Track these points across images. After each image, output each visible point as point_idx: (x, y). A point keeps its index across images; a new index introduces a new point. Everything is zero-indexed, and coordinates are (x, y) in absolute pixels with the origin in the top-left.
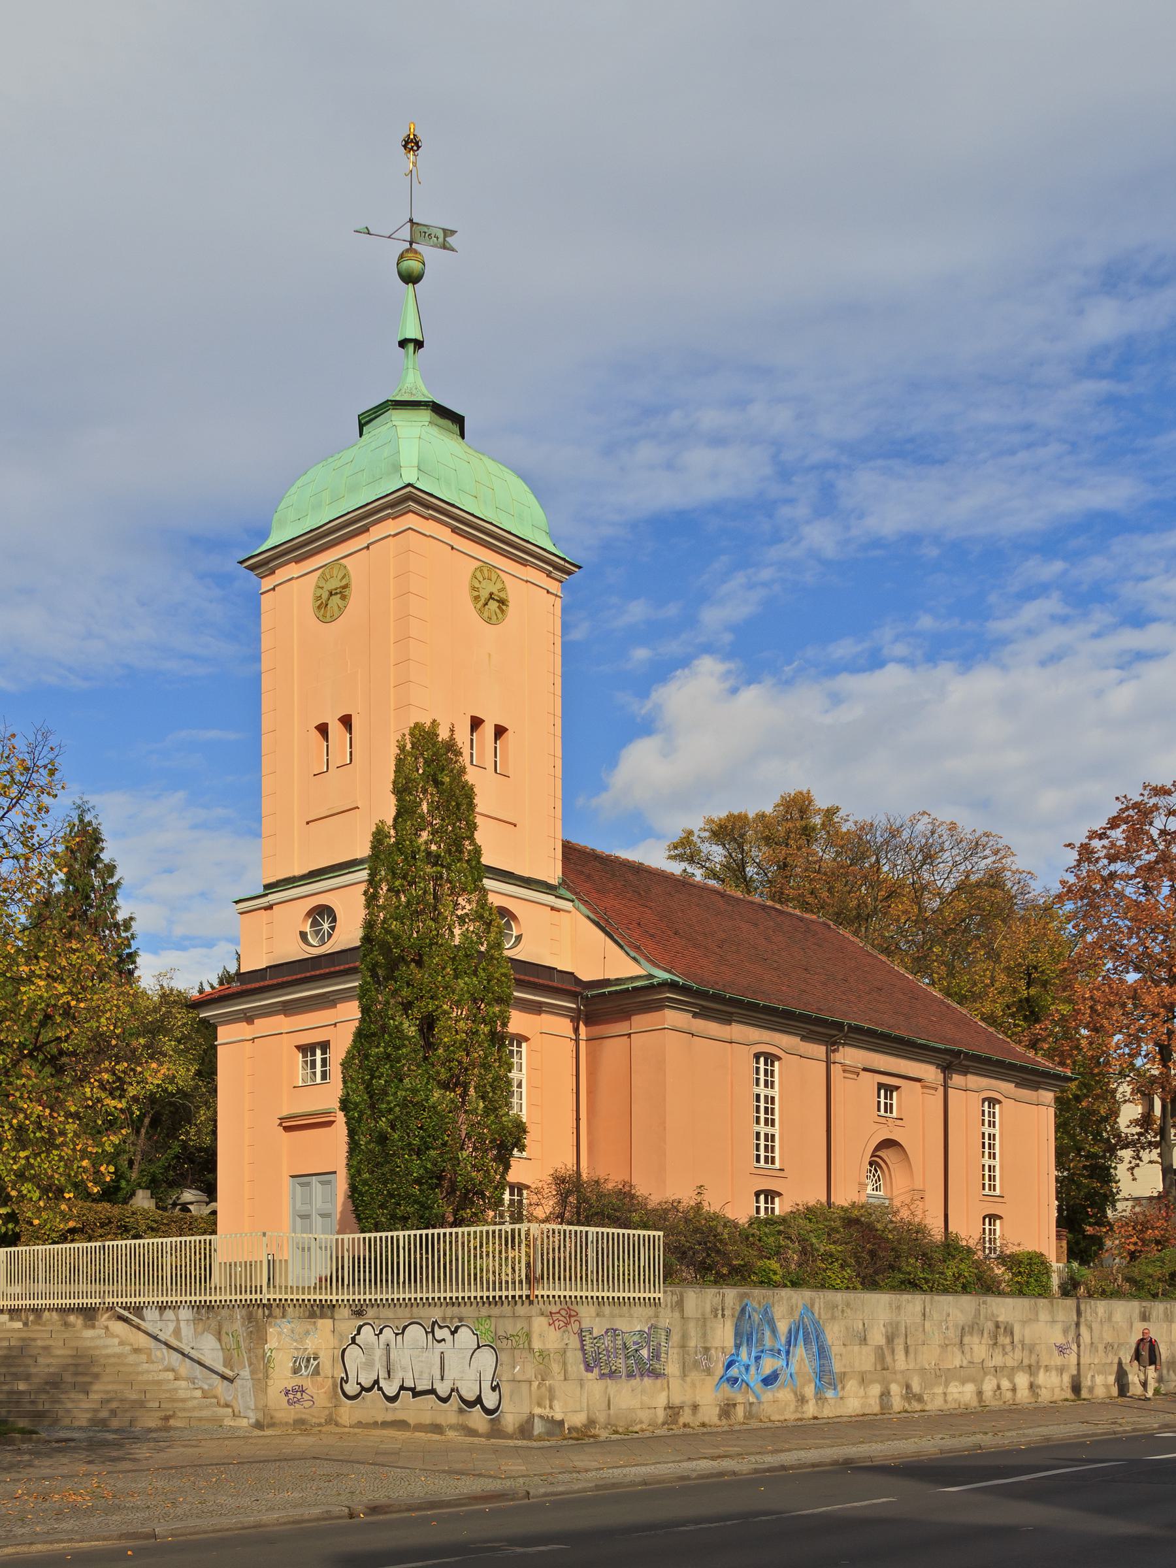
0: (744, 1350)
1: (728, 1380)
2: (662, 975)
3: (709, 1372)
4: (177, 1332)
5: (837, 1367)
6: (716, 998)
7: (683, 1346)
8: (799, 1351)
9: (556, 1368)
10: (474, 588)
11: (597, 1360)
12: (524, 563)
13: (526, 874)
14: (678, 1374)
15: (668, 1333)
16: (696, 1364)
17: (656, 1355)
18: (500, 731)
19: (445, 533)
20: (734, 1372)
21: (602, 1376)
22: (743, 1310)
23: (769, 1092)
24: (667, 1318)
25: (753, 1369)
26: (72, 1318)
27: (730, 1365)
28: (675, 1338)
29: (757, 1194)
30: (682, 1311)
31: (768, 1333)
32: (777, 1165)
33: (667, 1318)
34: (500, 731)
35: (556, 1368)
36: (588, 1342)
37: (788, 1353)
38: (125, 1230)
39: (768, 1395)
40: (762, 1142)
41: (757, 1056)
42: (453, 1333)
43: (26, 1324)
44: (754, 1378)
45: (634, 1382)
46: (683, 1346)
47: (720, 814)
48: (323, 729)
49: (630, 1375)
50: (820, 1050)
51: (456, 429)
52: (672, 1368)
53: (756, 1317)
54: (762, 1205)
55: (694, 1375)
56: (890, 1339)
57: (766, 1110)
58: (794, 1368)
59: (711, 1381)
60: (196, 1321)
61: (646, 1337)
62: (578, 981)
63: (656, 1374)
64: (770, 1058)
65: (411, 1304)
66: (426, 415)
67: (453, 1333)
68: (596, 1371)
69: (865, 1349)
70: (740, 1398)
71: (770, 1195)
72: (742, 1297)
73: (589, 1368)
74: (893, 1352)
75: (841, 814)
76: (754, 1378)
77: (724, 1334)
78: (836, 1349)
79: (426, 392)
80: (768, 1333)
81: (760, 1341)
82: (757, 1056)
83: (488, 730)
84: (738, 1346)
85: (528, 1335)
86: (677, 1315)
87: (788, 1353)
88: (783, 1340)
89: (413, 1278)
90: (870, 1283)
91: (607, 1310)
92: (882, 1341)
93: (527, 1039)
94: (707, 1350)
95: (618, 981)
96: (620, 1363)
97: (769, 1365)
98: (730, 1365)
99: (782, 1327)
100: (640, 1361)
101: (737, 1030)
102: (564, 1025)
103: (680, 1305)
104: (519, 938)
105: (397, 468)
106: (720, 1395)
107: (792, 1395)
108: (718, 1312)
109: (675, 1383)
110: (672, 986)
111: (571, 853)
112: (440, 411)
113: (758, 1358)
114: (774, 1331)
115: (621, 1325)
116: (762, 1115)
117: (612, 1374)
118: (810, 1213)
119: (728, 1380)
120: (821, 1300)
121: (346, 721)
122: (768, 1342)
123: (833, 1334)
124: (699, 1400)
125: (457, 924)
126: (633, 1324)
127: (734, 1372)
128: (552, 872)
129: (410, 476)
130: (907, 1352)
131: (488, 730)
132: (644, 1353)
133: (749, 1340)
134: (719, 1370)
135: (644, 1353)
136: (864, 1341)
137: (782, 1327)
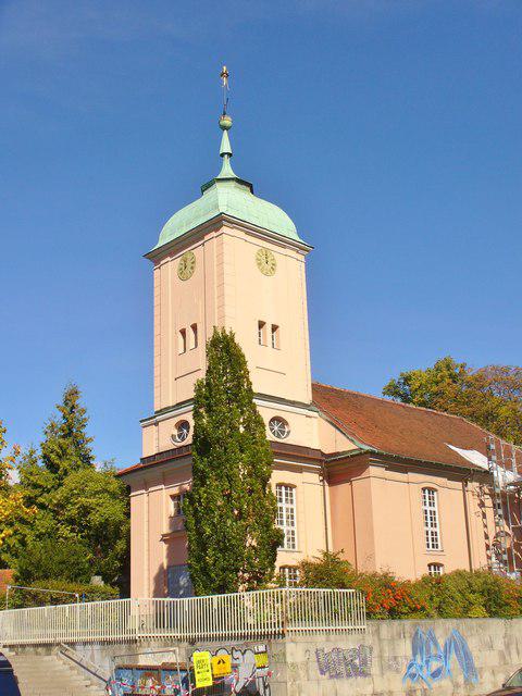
0: (418, 657)
1: (410, 675)
2: (367, 448)
3: (397, 671)
4: (92, 657)
5: (477, 664)
6: (398, 459)
7: (381, 657)
8: (453, 656)
9: (302, 673)
10: (258, 259)
11: (328, 667)
12: (284, 247)
13: (292, 399)
14: (378, 673)
15: (371, 649)
16: (390, 667)
17: (364, 662)
18: (274, 328)
19: (242, 234)
20: (413, 670)
21: (331, 677)
22: (417, 633)
23: (432, 509)
24: (369, 640)
25: (425, 668)
26: (40, 649)
27: (410, 666)
28: (376, 652)
29: (429, 566)
30: (379, 636)
31: (432, 646)
32: (440, 548)
33: (369, 640)
34: (274, 328)
35: (302, 673)
36: (321, 657)
37: (446, 657)
38: (85, 597)
39: (435, 684)
40: (430, 537)
41: (424, 489)
42: (243, 654)
43: (17, 654)
44: (425, 673)
45: (352, 679)
46: (381, 657)
47: (421, 364)
48: (183, 332)
49: (349, 675)
50: (459, 485)
51: (248, 189)
52: (375, 669)
53: (425, 637)
54: (433, 571)
55: (388, 674)
56: (507, 646)
57: (430, 519)
58: (450, 665)
59: (399, 677)
60: (102, 650)
61: (358, 652)
62: (323, 454)
63: (364, 674)
64: (432, 490)
65: (221, 638)
66: (233, 184)
67: (243, 654)
68: (327, 674)
69: (492, 652)
70: (418, 686)
71: (437, 566)
72: (415, 625)
73: (322, 672)
74: (510, 655)
75: (468, 366)
76: (425, 673)
77: (405, 648)
78: (475, 653)
79: (231, 172)
80: (432, 646)
81: (428, 651)
82: (424, 489)
83: (268, 328)
84: (414, 654)
85: (284, 654)
86: (376, 639)
87: (446, 657)
88: (442, 649)
89: (222, 624)
90: (493, 614)
91: (332, 637)
92: (502, 647)
93: (295, 487)
94: (395, 658)
95: (344, 453)
96: (342, 668)
97: (435, 665)
98: (410, 666)
99: (441, 642)
100: (354, 666)
101: (412, 476)
102: (316, 478)
103: (378, 632)
104: (289, 432)
105: (217, 207)
106: (406, 685)
107: (450, 684)
108: (401, 635)
109: (377, 680)
110: (372, 453)
111: (316, 388)
112: (238, 181)
113: (427, 662)
114: (436, 644)
115: (342, 645)
116: (429, 521)
117: (338, 676)
118: (459, 574)
119: (410, 675)
120: (463, 625)
121: (194, 327)
122: (433, 651)
123: (473, 644)
124: (392, 688)
125: (210, 430)
126: (348, 644)
127: (413, 670)
128: (307, 397)
129: (222, 209)
130: (518, 653)
131: (268, 328)
132: (357, 661)
133: (421, 649)
134: (404, 669)
135: (357, 661)
136: (491, 647)
137: (441, 642)
